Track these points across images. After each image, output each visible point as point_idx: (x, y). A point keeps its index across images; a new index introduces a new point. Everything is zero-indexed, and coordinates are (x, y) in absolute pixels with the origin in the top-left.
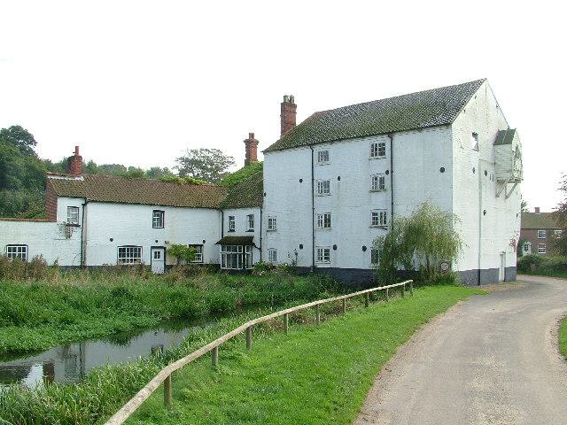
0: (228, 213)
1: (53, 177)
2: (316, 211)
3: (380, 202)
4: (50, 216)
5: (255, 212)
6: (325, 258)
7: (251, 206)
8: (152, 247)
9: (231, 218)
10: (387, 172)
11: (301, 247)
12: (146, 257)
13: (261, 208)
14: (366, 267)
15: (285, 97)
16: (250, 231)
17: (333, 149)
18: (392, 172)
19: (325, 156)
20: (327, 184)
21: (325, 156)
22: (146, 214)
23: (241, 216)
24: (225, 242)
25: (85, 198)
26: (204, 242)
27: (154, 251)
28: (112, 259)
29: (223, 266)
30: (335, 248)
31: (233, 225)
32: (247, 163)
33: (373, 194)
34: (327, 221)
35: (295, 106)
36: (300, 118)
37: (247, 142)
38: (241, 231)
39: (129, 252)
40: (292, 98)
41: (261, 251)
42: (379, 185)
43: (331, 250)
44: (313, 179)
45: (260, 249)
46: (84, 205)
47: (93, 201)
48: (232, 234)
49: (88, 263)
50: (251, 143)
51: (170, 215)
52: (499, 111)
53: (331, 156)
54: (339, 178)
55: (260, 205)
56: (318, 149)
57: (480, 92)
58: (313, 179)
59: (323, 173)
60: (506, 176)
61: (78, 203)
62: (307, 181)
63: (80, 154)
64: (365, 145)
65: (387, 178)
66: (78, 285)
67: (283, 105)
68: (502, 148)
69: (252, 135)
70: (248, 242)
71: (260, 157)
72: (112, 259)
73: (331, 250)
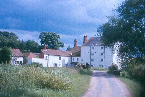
3: (92, 51)
5: (79, 57)
9: (73, 58)
11: (94, 65)
12: (58, 66)
13: (80, 56)
19: (93, 48)
20: (93, 53)
21: (93, 48)
28: (52, 66)
30: (94, 65)
31: (74, 60)
39: (55, 65)
42: (102, 54)
43: (94, 65)
46: (48, 56)
48: (73, 62)
56: (92, 47)
59: (92, 51)
61: (47, 55)
62: (90, 53)
65: (104, 54)
69: (76, 39)
72: (52, 66)
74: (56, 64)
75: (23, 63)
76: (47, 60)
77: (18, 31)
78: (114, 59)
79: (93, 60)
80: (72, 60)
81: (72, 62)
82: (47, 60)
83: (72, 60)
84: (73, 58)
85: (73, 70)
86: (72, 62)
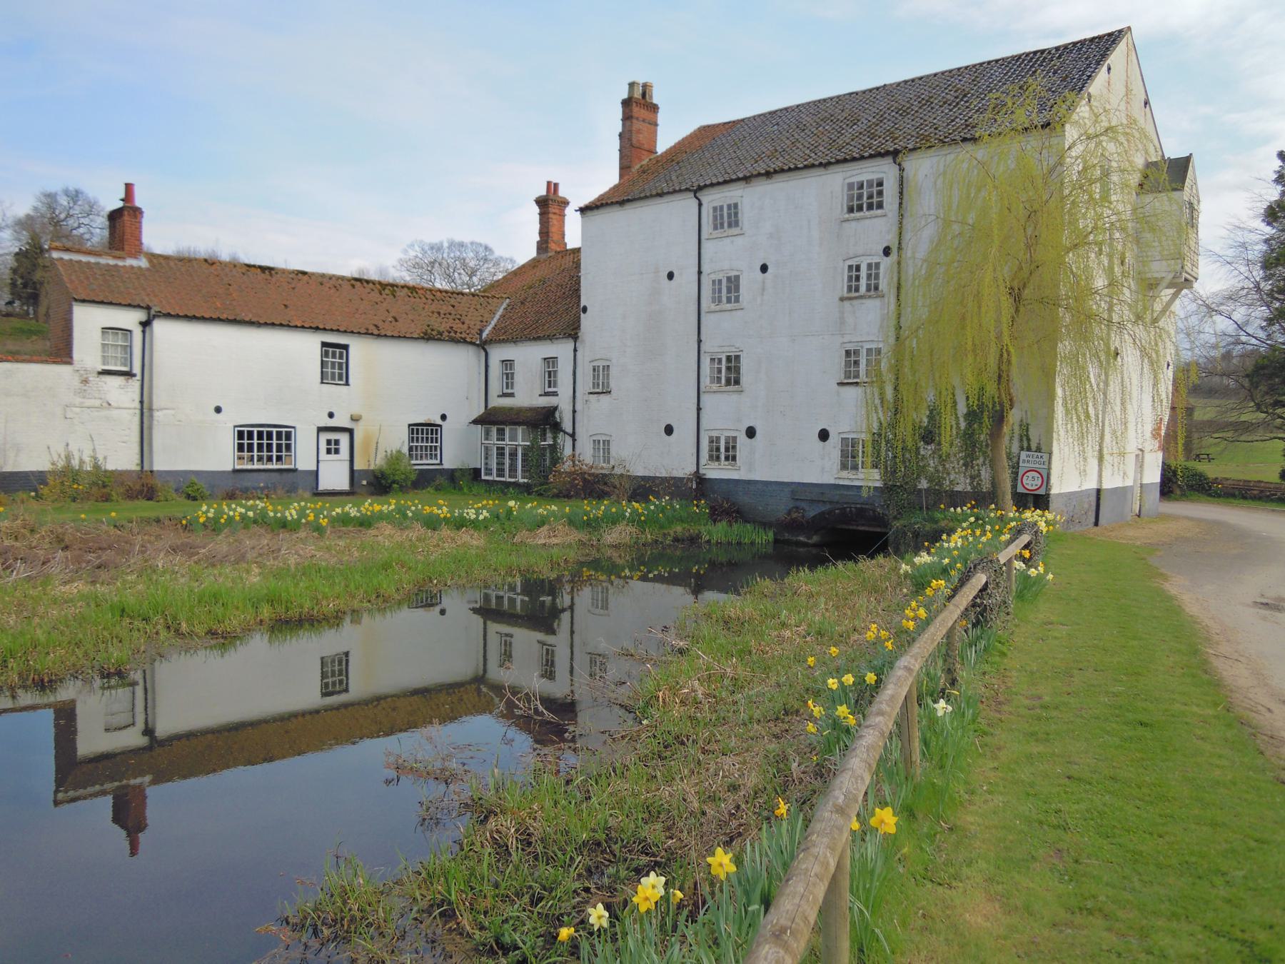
0: (498, 354)
1: (66, 256)
2: (704, 347)
4: (62, 352)
5: (561, 350)
6: (727, 458)
7: (551, 338)
8: (321, 430)
10: (887, 251)
12: (304, 456)
14: (78, 753)
15: (632, 85)
16: (547, 394)
17: (750, 198)
18: (900, 248)
19: (729, 219)
20: (734, 283)
22: (306, 347)
23: (528, 357)
24: (490, 419)
25: (148, 308)
26: (444, 417)
27: (324, 437)
29: (489, 472)
30: (751, 433)
31: (509, 377)
32: (542, 246)
33: (847, 303)
34: (731, 372)
35: (654, 108)
36: (666, 139)
37: (543, 203)
38: (527, 396)
40: (646, 88)
41: (574, 440)
44: (700, 273)
45: (573, 436)
46: (146, 324)
47: (168, 316)
49: (161, 463)
50: (550, 204)
51: (361, 351)
52: (1149, 115)
53: (746, 215)
54: (764, 268)
55: (572, 332)
56: (712, 199)
57: (1117, 57)
58: (700, 273)
60: (1159, 269)
61: (129, 319)
62: (687, 278)
63: (139, 202)
64: (834, 184)
66: (906, 664)
67: (626, 103)
68: (1160, 203)
70: (544, 420)
71: (573, 232)
73: (742, 438)
74: (288, 436)
75: (879, 526)
76: (135, 384)
77: (924, 639)
78: (736, 477)
79: (734, 379)
80: (495, 387)
81: (497, 410)
82: (135, 384)
83: (495, 387)
84: (508, 364)
85: (62, 463)
86: (496, 402)
